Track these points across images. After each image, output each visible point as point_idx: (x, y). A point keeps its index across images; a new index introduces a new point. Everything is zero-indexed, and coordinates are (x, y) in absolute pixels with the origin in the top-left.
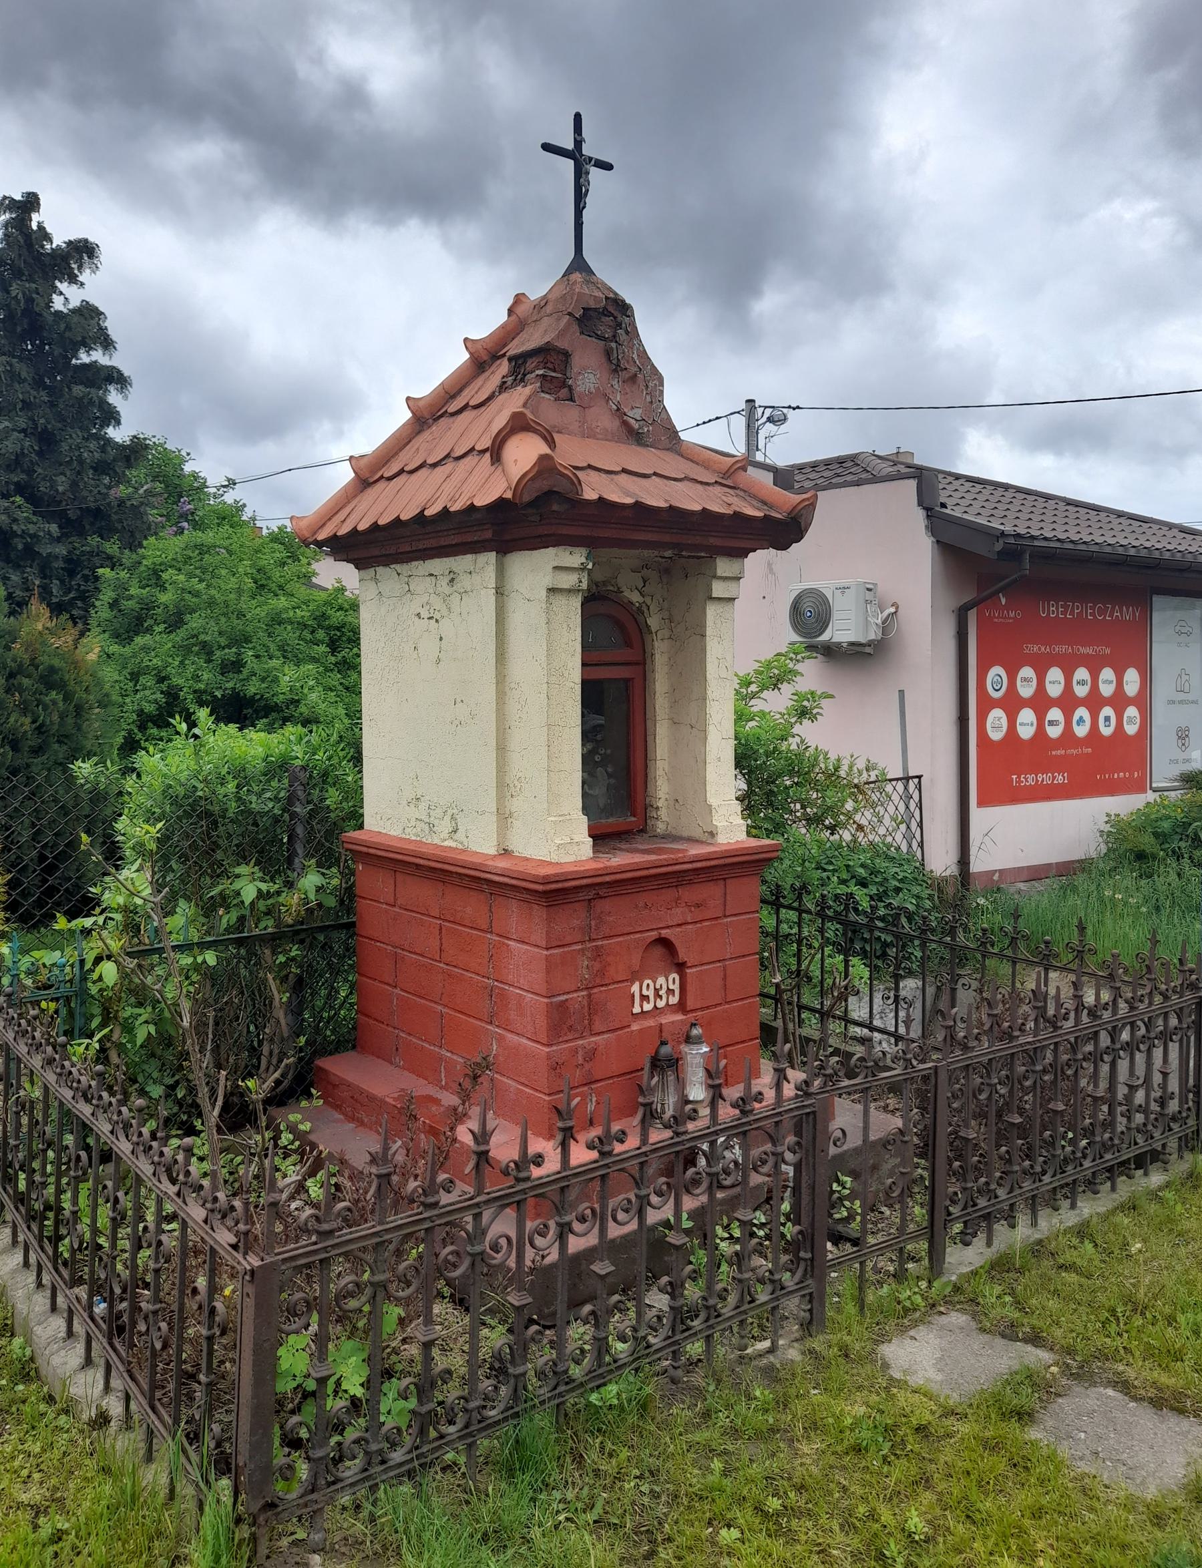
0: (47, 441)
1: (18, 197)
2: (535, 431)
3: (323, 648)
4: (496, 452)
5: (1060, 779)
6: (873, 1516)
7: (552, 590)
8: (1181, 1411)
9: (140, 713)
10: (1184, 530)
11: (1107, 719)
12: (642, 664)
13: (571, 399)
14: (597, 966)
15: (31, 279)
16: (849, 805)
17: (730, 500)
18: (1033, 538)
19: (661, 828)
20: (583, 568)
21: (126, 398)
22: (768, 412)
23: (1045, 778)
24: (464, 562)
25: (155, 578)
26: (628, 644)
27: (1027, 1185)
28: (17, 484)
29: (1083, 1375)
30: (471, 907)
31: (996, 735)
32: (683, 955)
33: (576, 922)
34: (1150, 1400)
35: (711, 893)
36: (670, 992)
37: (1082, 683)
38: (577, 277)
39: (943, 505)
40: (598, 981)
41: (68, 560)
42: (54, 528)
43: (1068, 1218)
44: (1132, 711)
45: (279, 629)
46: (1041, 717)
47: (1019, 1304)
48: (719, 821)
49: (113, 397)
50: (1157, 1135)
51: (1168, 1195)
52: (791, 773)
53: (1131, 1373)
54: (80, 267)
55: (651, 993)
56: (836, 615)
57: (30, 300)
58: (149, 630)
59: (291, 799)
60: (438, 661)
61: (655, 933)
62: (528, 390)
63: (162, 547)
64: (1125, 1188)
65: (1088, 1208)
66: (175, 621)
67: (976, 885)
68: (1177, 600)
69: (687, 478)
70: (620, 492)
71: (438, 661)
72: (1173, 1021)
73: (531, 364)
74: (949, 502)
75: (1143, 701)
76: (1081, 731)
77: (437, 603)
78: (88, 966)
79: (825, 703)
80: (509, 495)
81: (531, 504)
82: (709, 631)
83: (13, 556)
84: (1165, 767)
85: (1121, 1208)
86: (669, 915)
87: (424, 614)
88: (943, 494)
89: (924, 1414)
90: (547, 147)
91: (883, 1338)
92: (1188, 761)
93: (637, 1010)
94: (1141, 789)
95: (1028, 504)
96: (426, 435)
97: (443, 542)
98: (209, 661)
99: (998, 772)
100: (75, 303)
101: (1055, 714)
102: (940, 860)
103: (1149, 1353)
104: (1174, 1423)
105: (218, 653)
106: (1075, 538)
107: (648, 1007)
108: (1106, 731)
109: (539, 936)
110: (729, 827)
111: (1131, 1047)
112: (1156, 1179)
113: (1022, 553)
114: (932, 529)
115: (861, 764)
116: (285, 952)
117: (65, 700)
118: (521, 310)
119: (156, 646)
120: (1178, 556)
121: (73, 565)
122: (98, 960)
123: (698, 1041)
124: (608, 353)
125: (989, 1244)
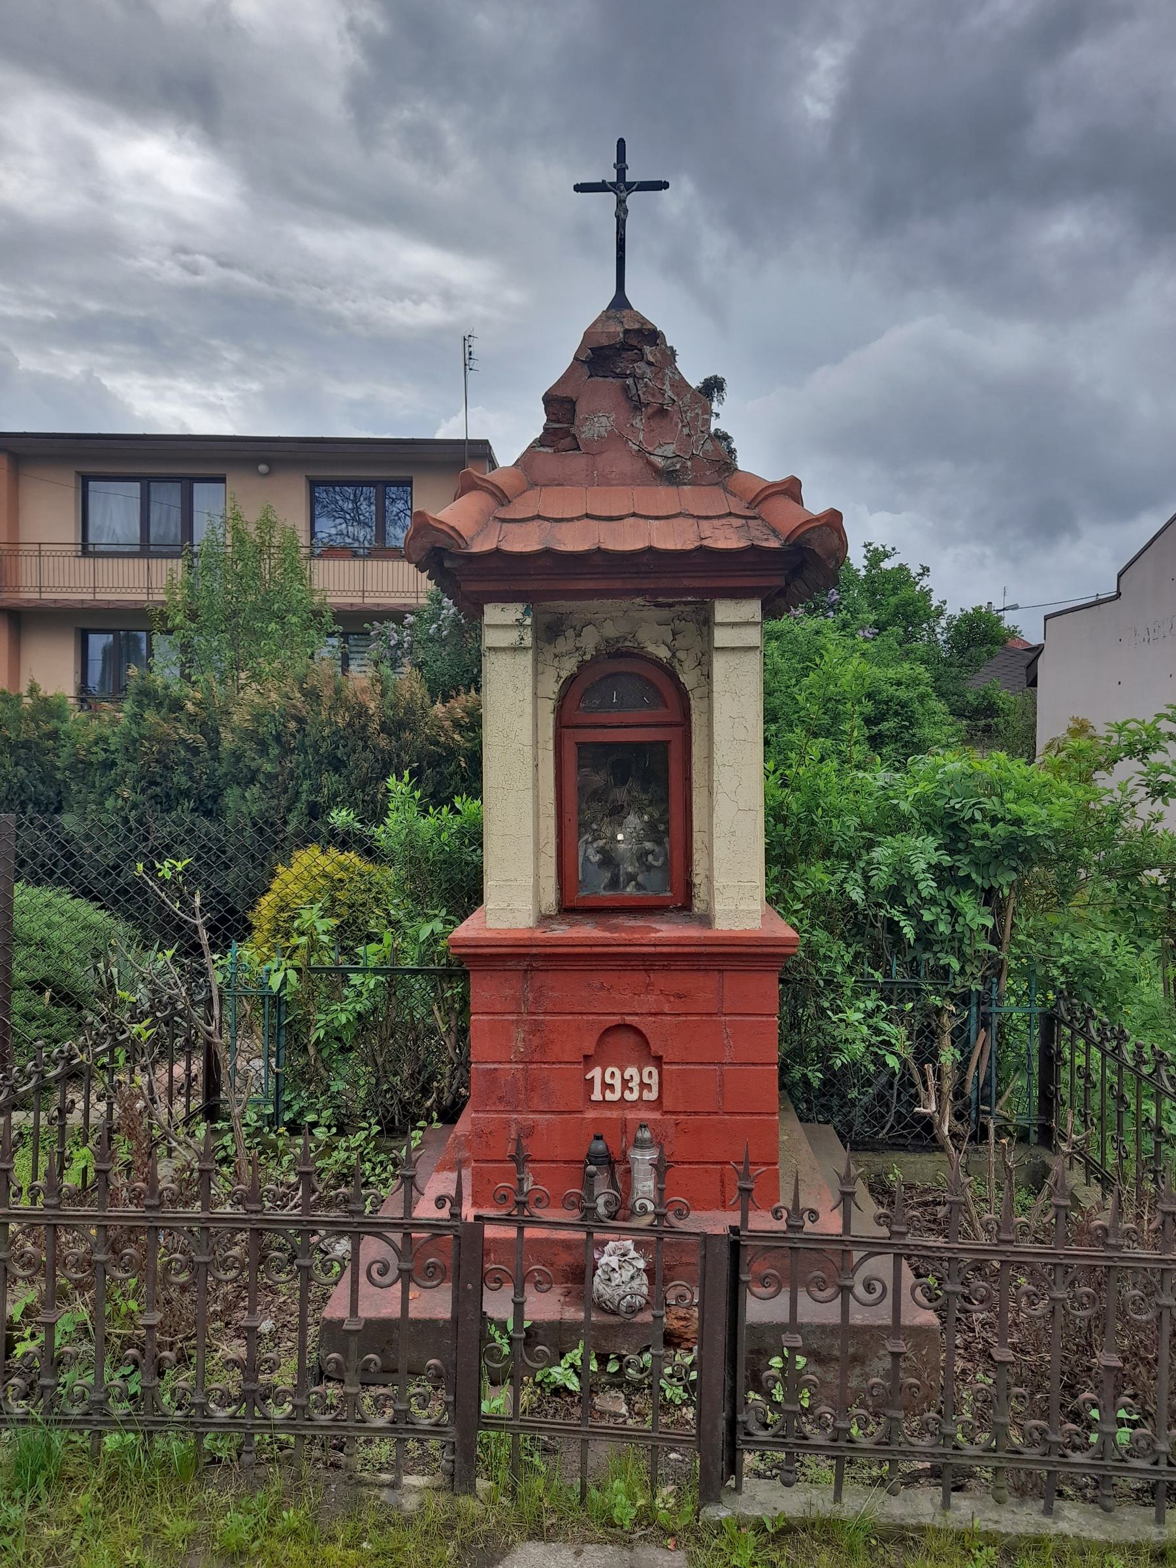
2: (482, 488)
13: (578, 448)
14: (536, 1041)
20: (520, 624)
32: (656, 1047)
33: (508, 992)
40: (537, 1057)
55: (617, 1083)
61: (618, 1017)
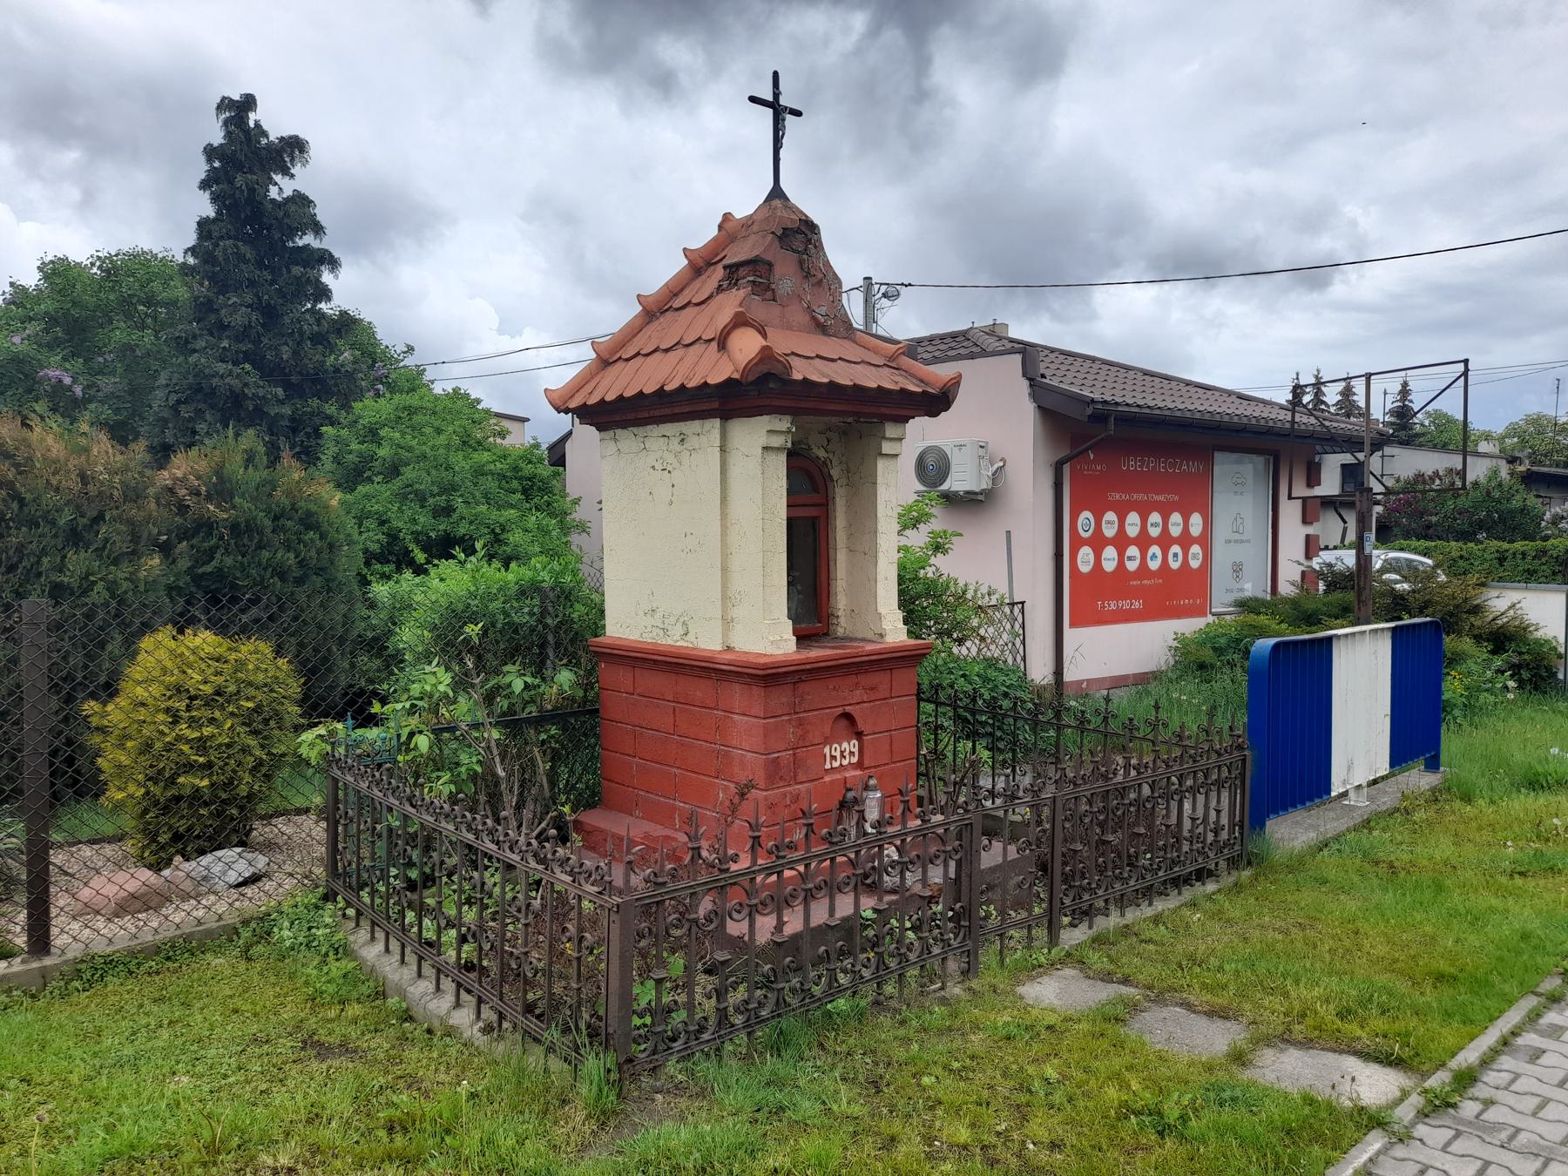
0: (270, 315)
1: (236, 97)
2: (752, 326)
3: (518, 496)
4: (722, 342)
5: (1137, 605)
6: (1021, 1069)
7: (765, 448)
8: (1226, 1018)
9: (366, 551)
10: (1241, 397)
11: (1175, 555)
12: (826, 504)
14: (800, 732)
15: (251, 172)
16: (975, 622)
17: (897, 379)
18: (1117, 404)
19: (840, 632)
21: (337, 277)
22: (883, 288)
23: (1125, 604)
24: (693, 426)
25: (373, 434)
26: (815, 489)
27: (1118, 886)
28: (245, 353)
29: (1160, 1000)
30: (700, 690)
31: (1085, 568)
32: (861, 726)
33: (784, 700)
34: (1205, 1013)
35: (880, 679)
36: (852, 753)
37: (1155, 525)
38: (777, 203)
39: (1043, 376)
41: (292, 419)
42: (280, 391)
43: (1148, 911)
44: (1196, 549)
45: (482, 479)
46: (1121, 554)
47: (1112, 961)
48: (887, 625)
49: (327, 278)
50: (1211, 855)
51: (1220, 897)
52: (928, 596)
53: (1192, 998)
54: (292, 160)
55: (838, 754)
56: (953, 468)
57: (252, 191)
58: (370, 480)
59: (544, 612)
60: (671, 503)
62: (742, 293)
63: (369, 409)
64: (1188, 893)
65: (1160, 905)
66: (393, 470)
67: (1068, 692)
68: (1235, 456)
69: (863, 362)
70: (819, 373)
71: (671, 503)
72: (1225, 773)
73: (742, 271)
74: (1047, 373)
75: (1205, 541)
76: (1154, 565)
77: (670, 458)
78: (403, 739)
79: (954, 539)
80: (736, 376)
81: (752, 383)
82: (879, 480)
83: (243, 414)
84: (1222, 596)
85: (1185, 905)
86: (850, 695)
87: (659, 466)
88: (1042, 365)
89: (1052, 1019)
90: (753, 99)
91: (1020, 983)
92: (1242, 590)
93: (828, 766)
94: (1202, 614)
95: (1112, 374)
96: (655, 325)
97: (676, 411)
98: (422, 507)
99: (1087, 599)
100: (288, 193)
101: (1133, 551)
102: (1040, 671)
103: (1204, 986)
104: (1220, 1023)
105: (431, 500)
106: (1151, 404)
107: (836, 764)
108: (1175, 565)
109: (758, 709)
110: (894, 631)
111: (1194, 791)
112: (1211, 887)
113: (1108, 416)
114: (1034, 396)
115: (984, 590)
116: (546, 731)
117: (321, 538)
118: (728, 226)
119: (378, 494)
120: (1236, 419)
121: (296, 425)
122: (411, 735)
123: (875, 789)
124: (801, 263)
125: (1090, 927)
